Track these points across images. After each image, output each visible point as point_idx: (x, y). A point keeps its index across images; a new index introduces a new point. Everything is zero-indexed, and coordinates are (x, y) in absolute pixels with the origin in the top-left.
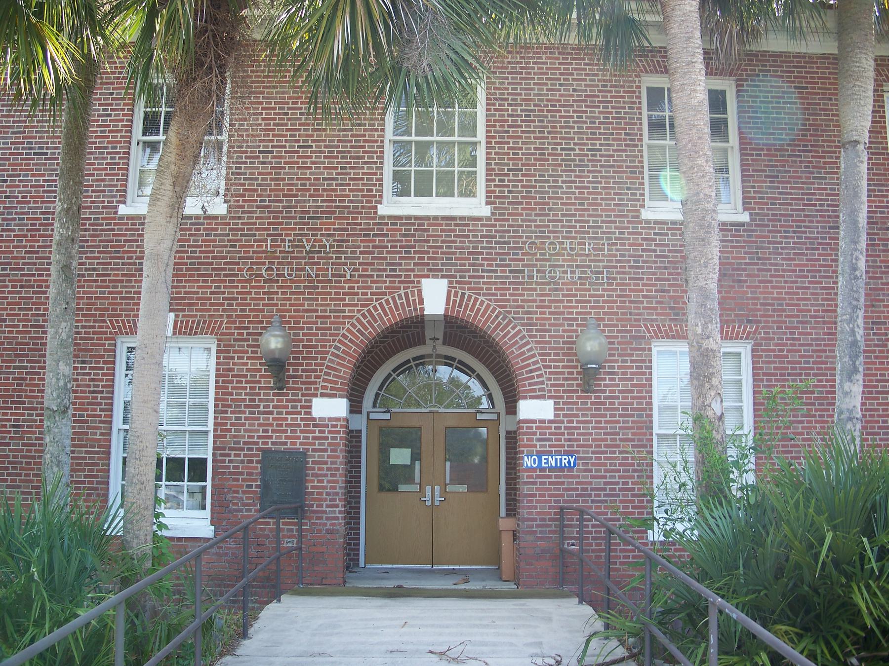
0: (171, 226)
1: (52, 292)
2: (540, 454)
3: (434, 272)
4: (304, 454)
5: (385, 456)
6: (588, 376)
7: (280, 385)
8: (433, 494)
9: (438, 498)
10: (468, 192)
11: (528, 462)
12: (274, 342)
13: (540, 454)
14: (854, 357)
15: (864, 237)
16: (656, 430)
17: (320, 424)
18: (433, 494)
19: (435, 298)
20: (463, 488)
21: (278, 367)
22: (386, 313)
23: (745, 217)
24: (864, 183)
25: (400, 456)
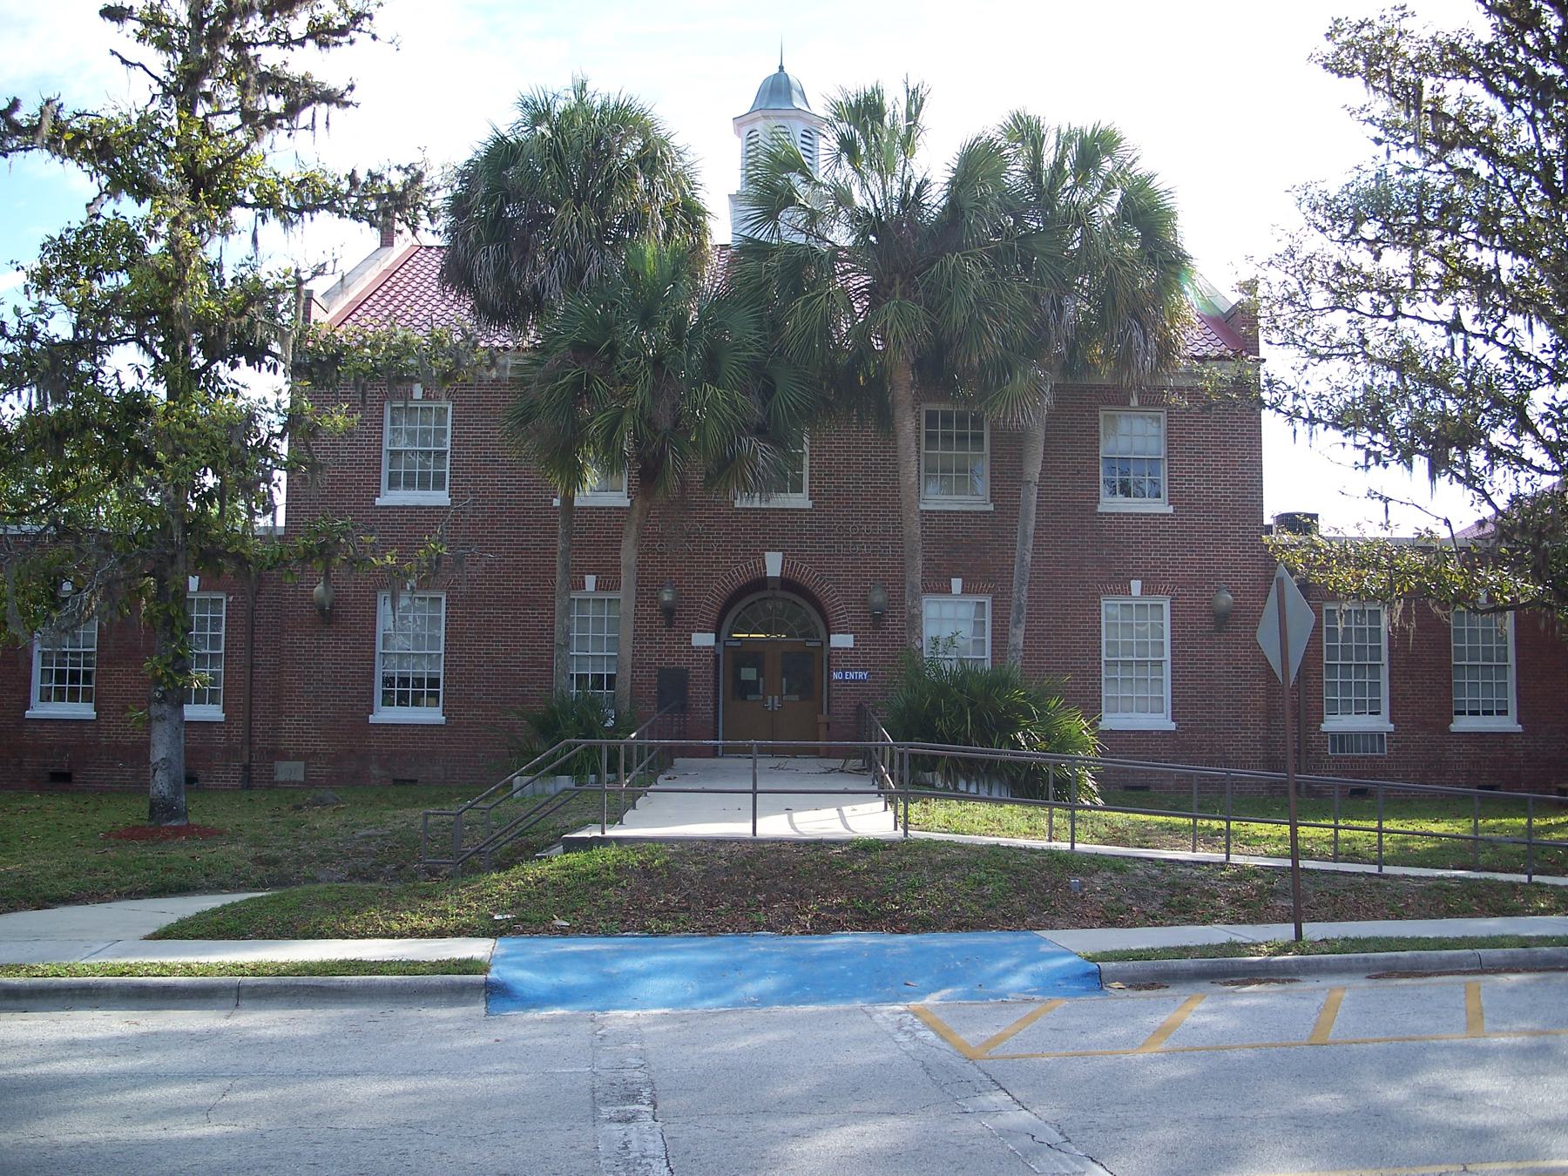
0: (114, 114)
1: (558, 578)
2: (844, 671)
3: (773, 548)
4: (687, 670)
5: (737, 675)
6: (877, 619)
7: (670, 624)
8: (773, 702)
9: (777, 704)
10: (798, 488)
11: (836, 676)
12: (667, 597)
13: (844, 671)
14: (1019, 613)
15: (1031, 541)
16: (1104, 658)
17: (698, 650)
18: (773, 702)
19: (774, 564)
20: (796, 698)
21: (669, 612)
22: (741, 575)
23: (991, 507)
24: (1034, 508)
25: (748, 674)
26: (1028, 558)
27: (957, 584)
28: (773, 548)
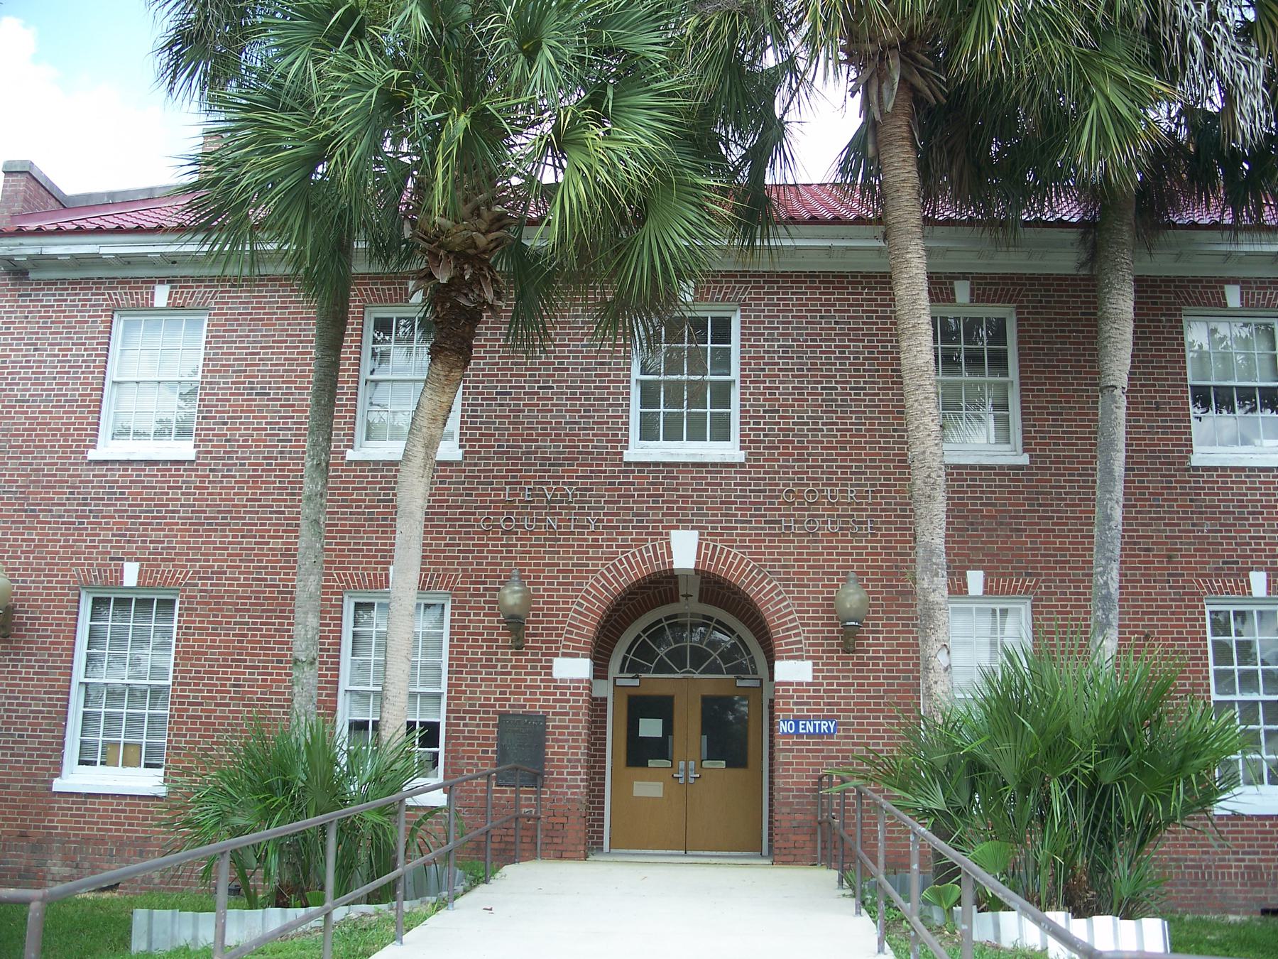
5: (668, 729)
17: (562, 686)
23: (1024, 460)
25: (650, 728)
26: (1118, 513)
27: (975, 580)
28: (684, 523)
